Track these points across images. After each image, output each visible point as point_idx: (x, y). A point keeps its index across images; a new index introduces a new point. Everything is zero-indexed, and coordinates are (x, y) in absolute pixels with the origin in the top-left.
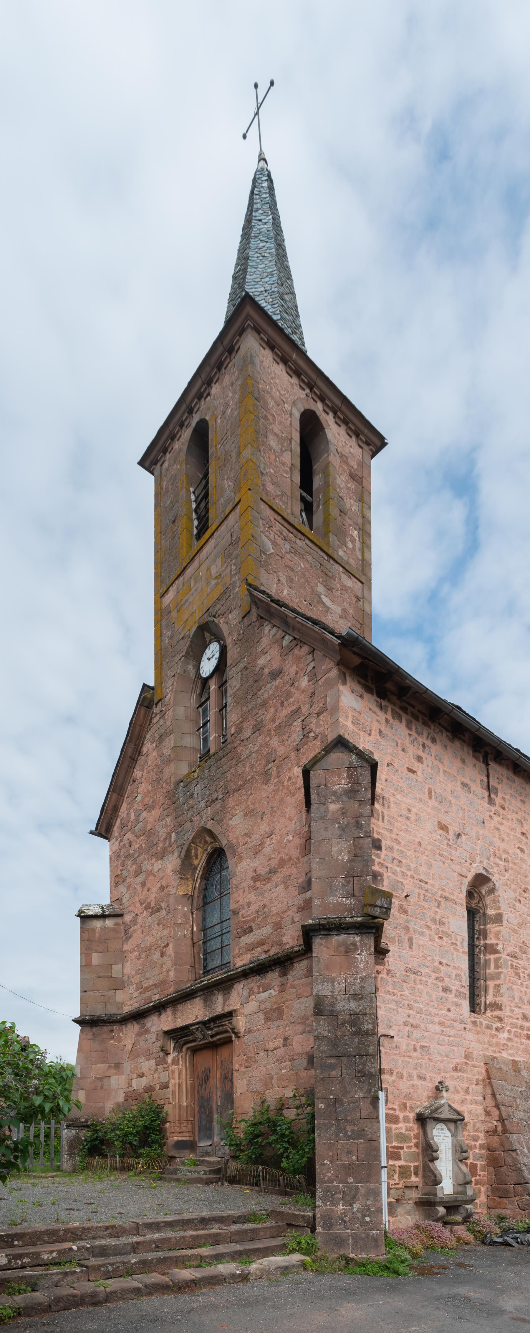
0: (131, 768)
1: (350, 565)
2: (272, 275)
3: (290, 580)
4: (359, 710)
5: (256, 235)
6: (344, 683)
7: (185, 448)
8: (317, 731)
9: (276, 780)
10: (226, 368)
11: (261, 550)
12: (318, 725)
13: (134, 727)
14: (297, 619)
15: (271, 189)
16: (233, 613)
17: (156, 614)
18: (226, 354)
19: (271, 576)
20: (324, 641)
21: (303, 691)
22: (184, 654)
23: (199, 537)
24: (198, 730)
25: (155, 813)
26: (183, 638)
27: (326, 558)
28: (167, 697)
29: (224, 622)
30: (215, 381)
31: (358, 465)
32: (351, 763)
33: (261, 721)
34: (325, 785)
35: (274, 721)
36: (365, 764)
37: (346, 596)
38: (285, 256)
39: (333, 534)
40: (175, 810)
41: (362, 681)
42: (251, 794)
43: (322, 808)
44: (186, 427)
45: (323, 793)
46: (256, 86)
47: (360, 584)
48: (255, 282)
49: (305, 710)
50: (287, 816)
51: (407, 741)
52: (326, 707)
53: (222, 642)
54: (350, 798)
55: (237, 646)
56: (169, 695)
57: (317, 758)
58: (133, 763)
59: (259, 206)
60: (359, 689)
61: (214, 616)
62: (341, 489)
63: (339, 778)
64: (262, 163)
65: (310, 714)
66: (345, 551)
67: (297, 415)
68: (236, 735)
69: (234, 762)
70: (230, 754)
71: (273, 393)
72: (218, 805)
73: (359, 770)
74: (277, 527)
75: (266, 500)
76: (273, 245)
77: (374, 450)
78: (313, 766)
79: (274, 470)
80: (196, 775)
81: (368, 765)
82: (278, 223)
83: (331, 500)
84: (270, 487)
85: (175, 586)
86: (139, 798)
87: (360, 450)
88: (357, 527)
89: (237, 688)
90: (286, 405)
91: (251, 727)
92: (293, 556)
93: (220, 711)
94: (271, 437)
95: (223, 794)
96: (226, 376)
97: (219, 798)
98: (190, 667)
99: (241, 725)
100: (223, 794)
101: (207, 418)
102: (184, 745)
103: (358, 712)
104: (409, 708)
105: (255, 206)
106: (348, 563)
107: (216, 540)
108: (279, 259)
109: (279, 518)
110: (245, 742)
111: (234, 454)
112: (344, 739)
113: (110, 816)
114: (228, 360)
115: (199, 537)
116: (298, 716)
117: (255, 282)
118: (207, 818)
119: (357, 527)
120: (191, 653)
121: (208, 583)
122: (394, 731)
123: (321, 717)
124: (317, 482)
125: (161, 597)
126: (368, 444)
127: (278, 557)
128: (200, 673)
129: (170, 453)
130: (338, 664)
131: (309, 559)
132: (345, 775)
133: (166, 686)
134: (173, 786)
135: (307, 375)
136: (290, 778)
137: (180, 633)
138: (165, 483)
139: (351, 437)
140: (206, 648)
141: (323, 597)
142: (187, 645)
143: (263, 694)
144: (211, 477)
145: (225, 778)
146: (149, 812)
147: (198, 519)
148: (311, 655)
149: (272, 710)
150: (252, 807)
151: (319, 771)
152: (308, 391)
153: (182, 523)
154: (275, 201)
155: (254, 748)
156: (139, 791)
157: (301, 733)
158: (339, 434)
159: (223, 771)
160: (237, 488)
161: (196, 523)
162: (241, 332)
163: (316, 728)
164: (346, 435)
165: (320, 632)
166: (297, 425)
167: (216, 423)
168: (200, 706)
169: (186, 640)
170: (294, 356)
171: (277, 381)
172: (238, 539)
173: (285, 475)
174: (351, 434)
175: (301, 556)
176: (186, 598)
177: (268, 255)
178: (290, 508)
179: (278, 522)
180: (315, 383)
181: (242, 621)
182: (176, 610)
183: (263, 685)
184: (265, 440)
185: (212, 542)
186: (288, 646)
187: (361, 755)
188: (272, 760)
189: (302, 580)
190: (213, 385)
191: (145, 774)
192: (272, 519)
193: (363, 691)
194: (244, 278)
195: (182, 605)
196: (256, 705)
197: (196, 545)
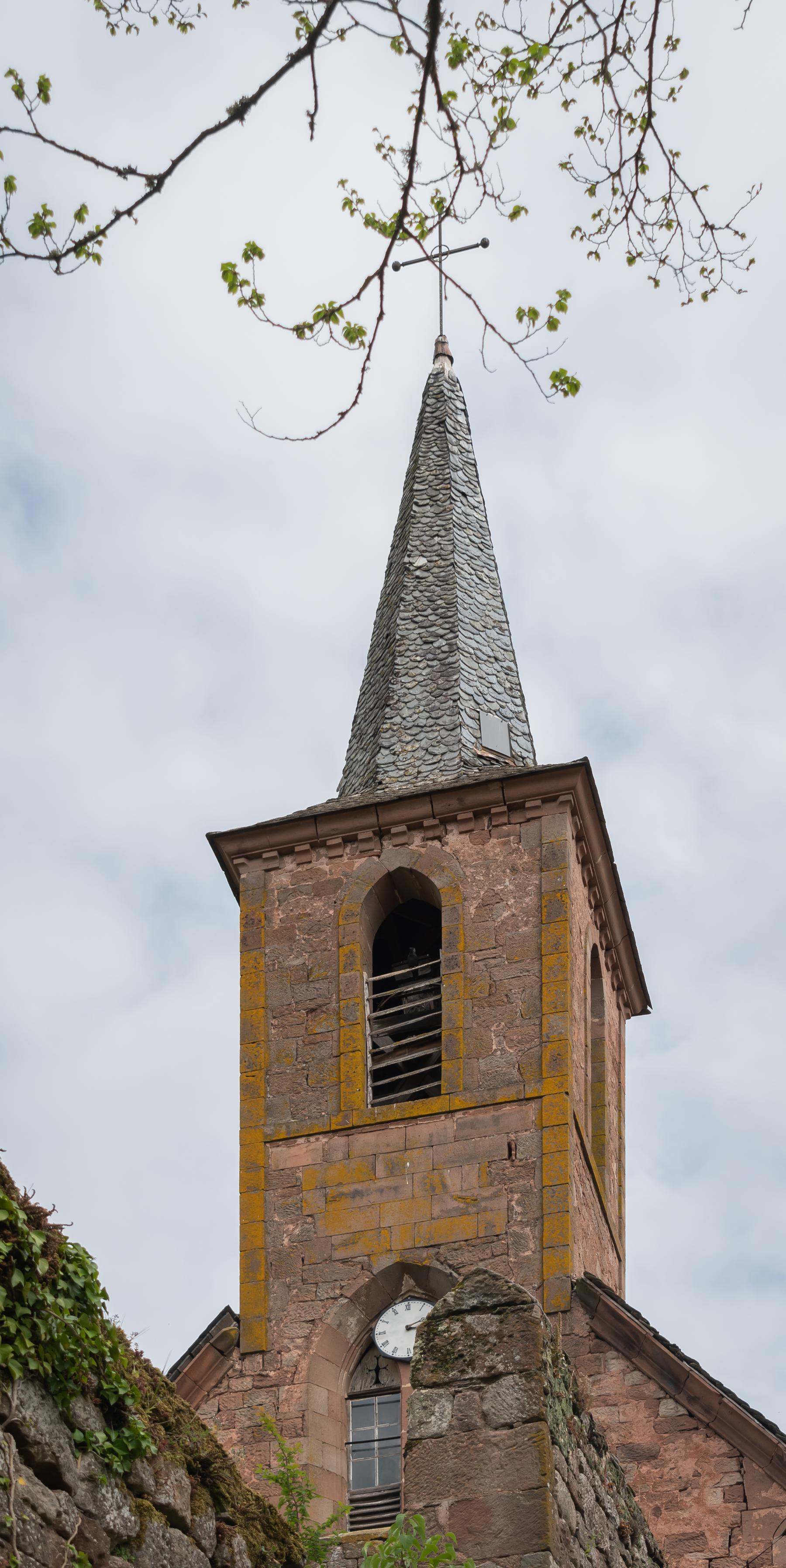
22: (349, 1295)
26: (344, 1261)
98: (352, 1321)
102: (325, 1467)
120: (363, 1298)
170: (600, 859)
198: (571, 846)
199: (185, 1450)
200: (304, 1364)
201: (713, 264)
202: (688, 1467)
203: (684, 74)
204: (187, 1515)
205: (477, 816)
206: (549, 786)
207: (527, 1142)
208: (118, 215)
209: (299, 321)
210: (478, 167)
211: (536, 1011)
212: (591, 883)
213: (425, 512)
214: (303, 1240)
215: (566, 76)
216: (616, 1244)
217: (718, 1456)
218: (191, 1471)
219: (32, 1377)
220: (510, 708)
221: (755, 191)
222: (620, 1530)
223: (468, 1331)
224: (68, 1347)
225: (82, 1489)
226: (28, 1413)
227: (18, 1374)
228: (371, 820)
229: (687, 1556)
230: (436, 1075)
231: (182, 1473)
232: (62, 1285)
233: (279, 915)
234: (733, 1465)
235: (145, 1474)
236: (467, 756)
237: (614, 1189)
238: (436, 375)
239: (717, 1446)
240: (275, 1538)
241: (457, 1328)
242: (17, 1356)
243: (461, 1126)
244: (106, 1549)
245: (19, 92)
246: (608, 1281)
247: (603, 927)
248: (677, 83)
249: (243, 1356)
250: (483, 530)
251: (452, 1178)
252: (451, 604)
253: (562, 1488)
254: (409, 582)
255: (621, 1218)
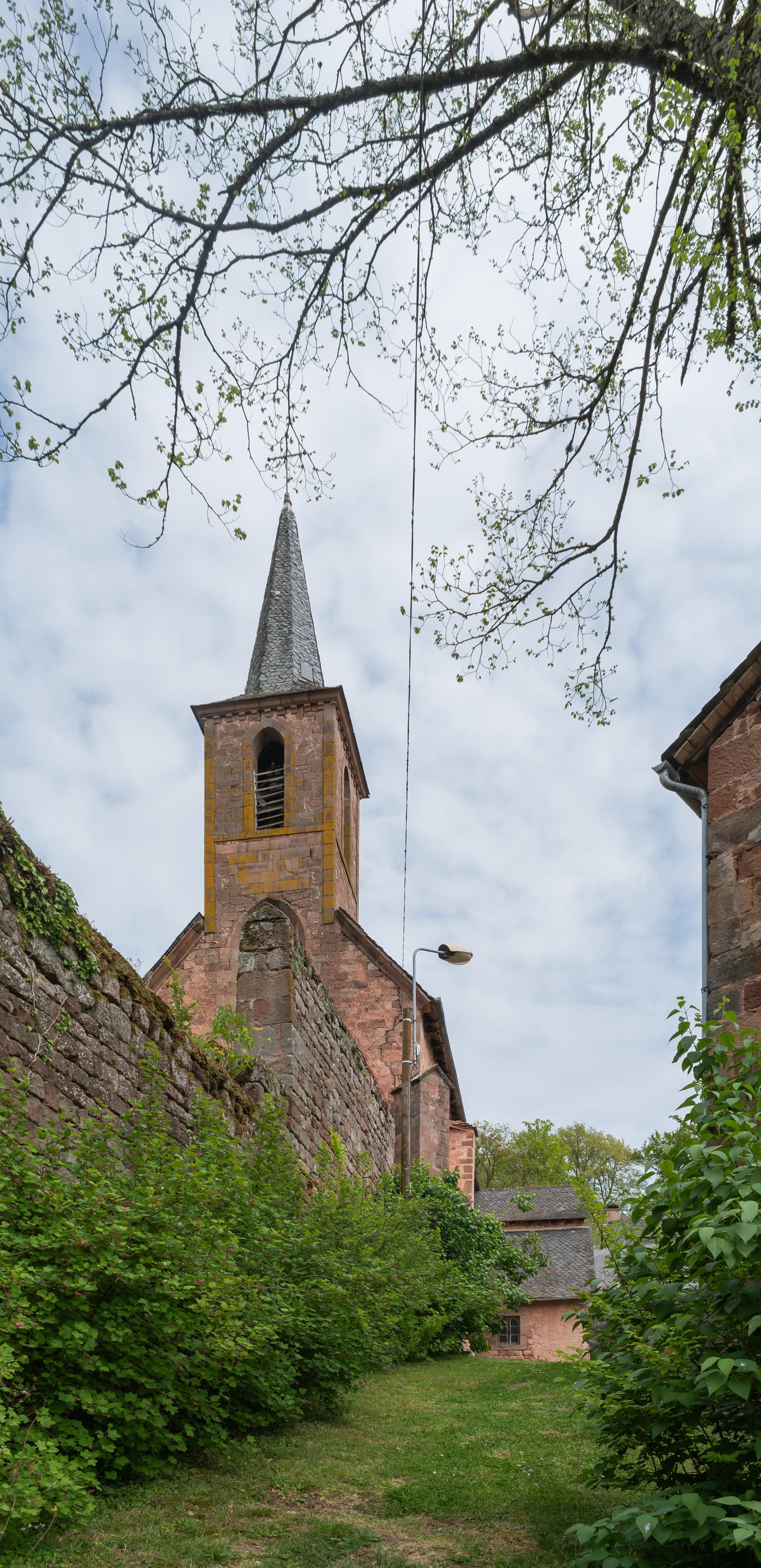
198: (336, 723)
199: (117, 971)
200: (230, 939)
201: (318, 485)
202: (378, 992)
203: (308, 402)
204: (118, 999)
205: (299, 707)
206: (327, 696)
207: (317, 848)
208: (60, 444)
209: (140, 496)
210: (209, 437)
211: (321, 794)
212: (345, 740)
213: (280, 571)
214: (229, 886)
215: (262, 398)
216: (355, 895)
218: (120, 980)
219: (42, 937)
220: (313, 661)
221: (333, 456)
222: (326, 1016)
223: (261, 929)
224: (57, 925)
225: (67, 985)
226: (41, 952)
227: (35, 935)
228: (256, 705)
230: (282, 818)
231: (116, 981)
232: (57, 899)
233: (220, 744)
234: (396, 992)
235: (98, 980)
236: (295, 680)
237: (354, 872)
238: (285, 510)
239: (390, 984)
240: (161, 1010)
241: (257, 927)
242: (34, 927)
243: (292, 841)
244: (79, 1010)
245: (19, 387)
246: (351, 913)
247: (350, 759)
248: (306, 405)
249: (206, 934)
250: (303, 581)
251: (288, 862)
252: (290, 613)
253: (298, 997)
254: (273, 602)
255: (357, 885)
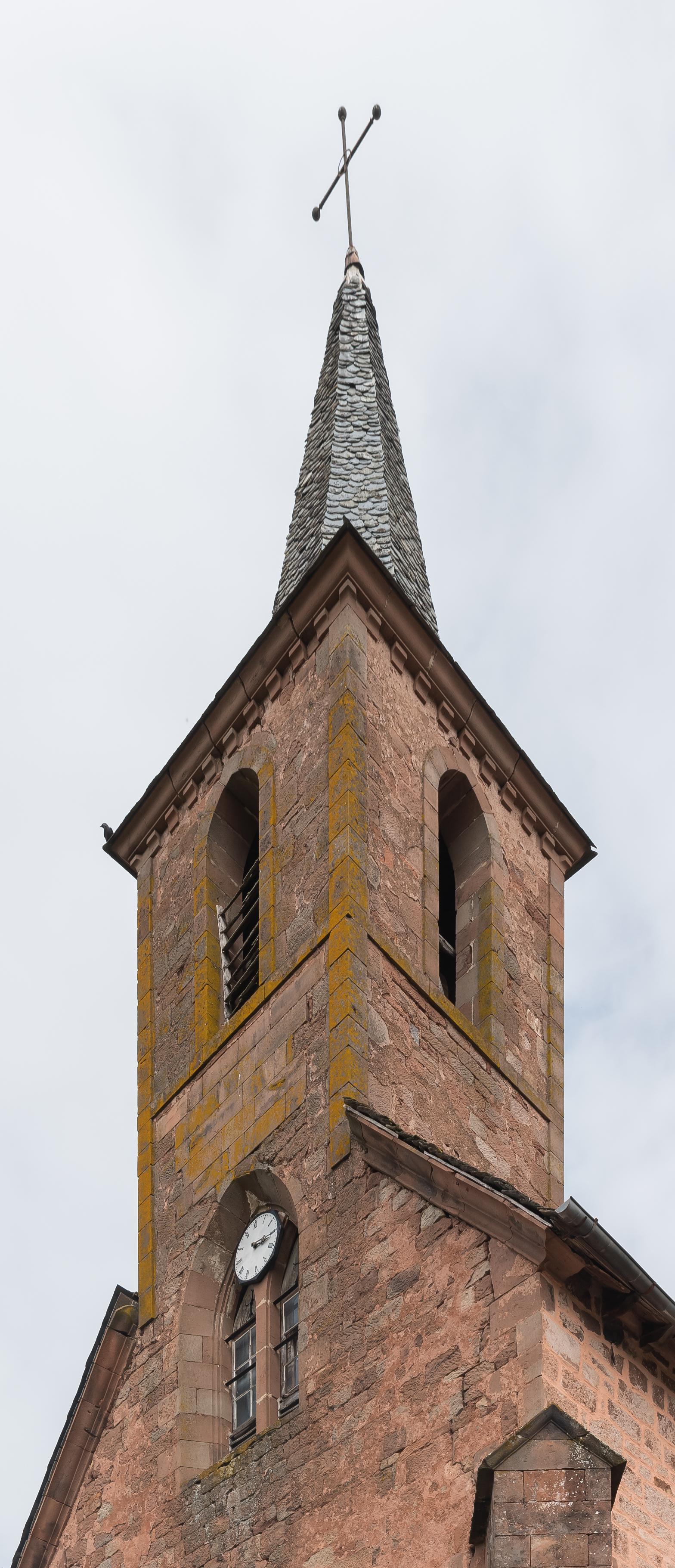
0: (87, 1451)
1: (527, 1084)
2: (379, 497)
3: (421, 1101)
4: (575, 1361)
5: (346, 414)
6: (551, 1307)
7: (206, 825)
8: (495, 1396)
9: (405, 1488)
10: (296, 671)
11: (369, 1038)
12: (496, 1385)
13: (97, 1372)
14: (457, 1176)
15: (372, 325)
16: (310, 1157)
17: (141, 1152)
18: (299, 642)
19: (387, 1090)
20: (514, 1223)
21: (465, 1318)
22: (203, 1232)
23: (234, 1004)
24: (227, 1385)
25: (141, 1542)
26: (200, 1202)
27: (485, 1066)
28: (167, 1315)
29: (292, 1174)
30: (272, 694)
31: (541, 890)
32: (573, 1461)
33: (373, 1372)
34: (523, 1501)
35: (400, 1372)
36: (601, 1464)
37: (519, 1143)
38: (401, 462)
39: (498, 1020)
40: (183, 1537)
41: (581, 1306)
42: (351, 1512)
43: (518, 1545)
44: (209, 783)
45: (520, 1516)
46: (342, 114)
47: (544, 1123)
48: (344, 506)
49: (467, 1354)
50: (429, 1557)
51: (656, 1427)
52: (515, 1351)
53: (283, 1215)
54: (571, 1528)
55: (320, 1222)
56: (171, 1311)
57: (510, 1448)
58: (91, 1442)
59: (349, 356)
60: (575, 1319)
61: (270, 1162)
62: (511, 933)
63: (551, 1489)
64: (353, 272)
65: (479, 1363)
66: (517, 1056)
67: (434, 779)
68: (317, 1396)
69: (313, 1449)
70: (304, 1434)
71: (390, 730)
72: (278, 1532)
73: (589, 1474)
74: (398, 995)
75: (378, 942)
76: (379, 438)
77: (570, 864)
78: (499, 1463)
79: (392, 883)
80: (230, 1470)
81: (606, 1466)
82: (386, 396)
83: (493, 953)
84: (386, 917)
85: (183, 1097)
86: (104, 1511)
87: (545, 862)
88: (539, 1011)
89: (320, 1304)
90: (414, 758)
91: (351, 1383)
92: (426, 1055)
93: (276, 1349)
94: (387, 817)
95: (288, 1510)
96: (297, 687)
97: (281, 1517)
98: (215, 1260)
99: (328, 1378)
100: (288, 1510)
101: (255, 768)
102: (200, 1412)
103: (574, 1364)
104: (659, 1363)
105: (341, 356)
106: (522, 1078)
107: (274, 1012)
108: (390, 467)
109: (401, 978)
110: (338, 1412)
111: (314, 845)
112: (562, 1413)
113: (41, 1542)
114: (302, 656)
115: (234, 1004)
116: (454, 1366)
117: (344, 506)
118: (254, 1555)
119: (539, 1011)
120: (218, 1232)
121: (256, 1095)
122: (633, 1406)
123: (503, 1370)
124: (465, 916)
125: (153, 1118)
126: (560, 852)
127: (398, 1055)
128: (234, 1271)
129: (171, 832)
130: (540, 1270)
131: (454, 1065)
132: (562, 1484)
133: (163, 1293)
134: (178, 1491)
135: (453, 703)
136: (435, 1485)
137: (195, 1192)
138: (161, 891)
139: (529, 834)
140: (248, 1224)
141: (478, 1140)
142: (211, 1215)
143: (376, 1320)
144: (265, 886)
145: (294, 1479)
146: (125, 1539)
147: (231, 968)
148: (482, 1248)
149: (396, 1351)
150: (352, 1537)
151: (512, 1473)
152: (453, 734)
153: (199, 973)
154: (380, 350)
155: (357, 1424)
156: (104, 1497)
157: (459, 1398)
158: (507, 826)
159: (289, 1466)
160: (321, 913)
161: (227, 976)
162: (332, 601)
163: (492, 1391)
164: (520, 828)
165: (506, 1203)
166: (433, 798)
167: (274, 780)
168: (233, 1337)
169: (208, 1205)
170: (431, 661)
171: (398, 708)
172: (323, 1013)
173: (412, 895)
174: (530, 828)
175: (441, 1057)
176: (208, 1122)
177: (369, 457)
178: (420, 961)
179: (400, 986)
180: (467, 721)
181: (331, 1175)
182: (185, 1145)
183: (377, 1302)
184: (376, 821)
185: (265, 1015)
186: (431, 1227)
187: (593, 1445)
188: (397, 1449)
189: (443, 1105)
190: (267, 702)
191: (116, 1464)
192: (389, 980)
193: (582, 1324)
194: (323, 497)
195: (200, 1136)
196: (362, 1341)
197: (228, 1023)
217: (468, 1250)
229: (444, 1381)
